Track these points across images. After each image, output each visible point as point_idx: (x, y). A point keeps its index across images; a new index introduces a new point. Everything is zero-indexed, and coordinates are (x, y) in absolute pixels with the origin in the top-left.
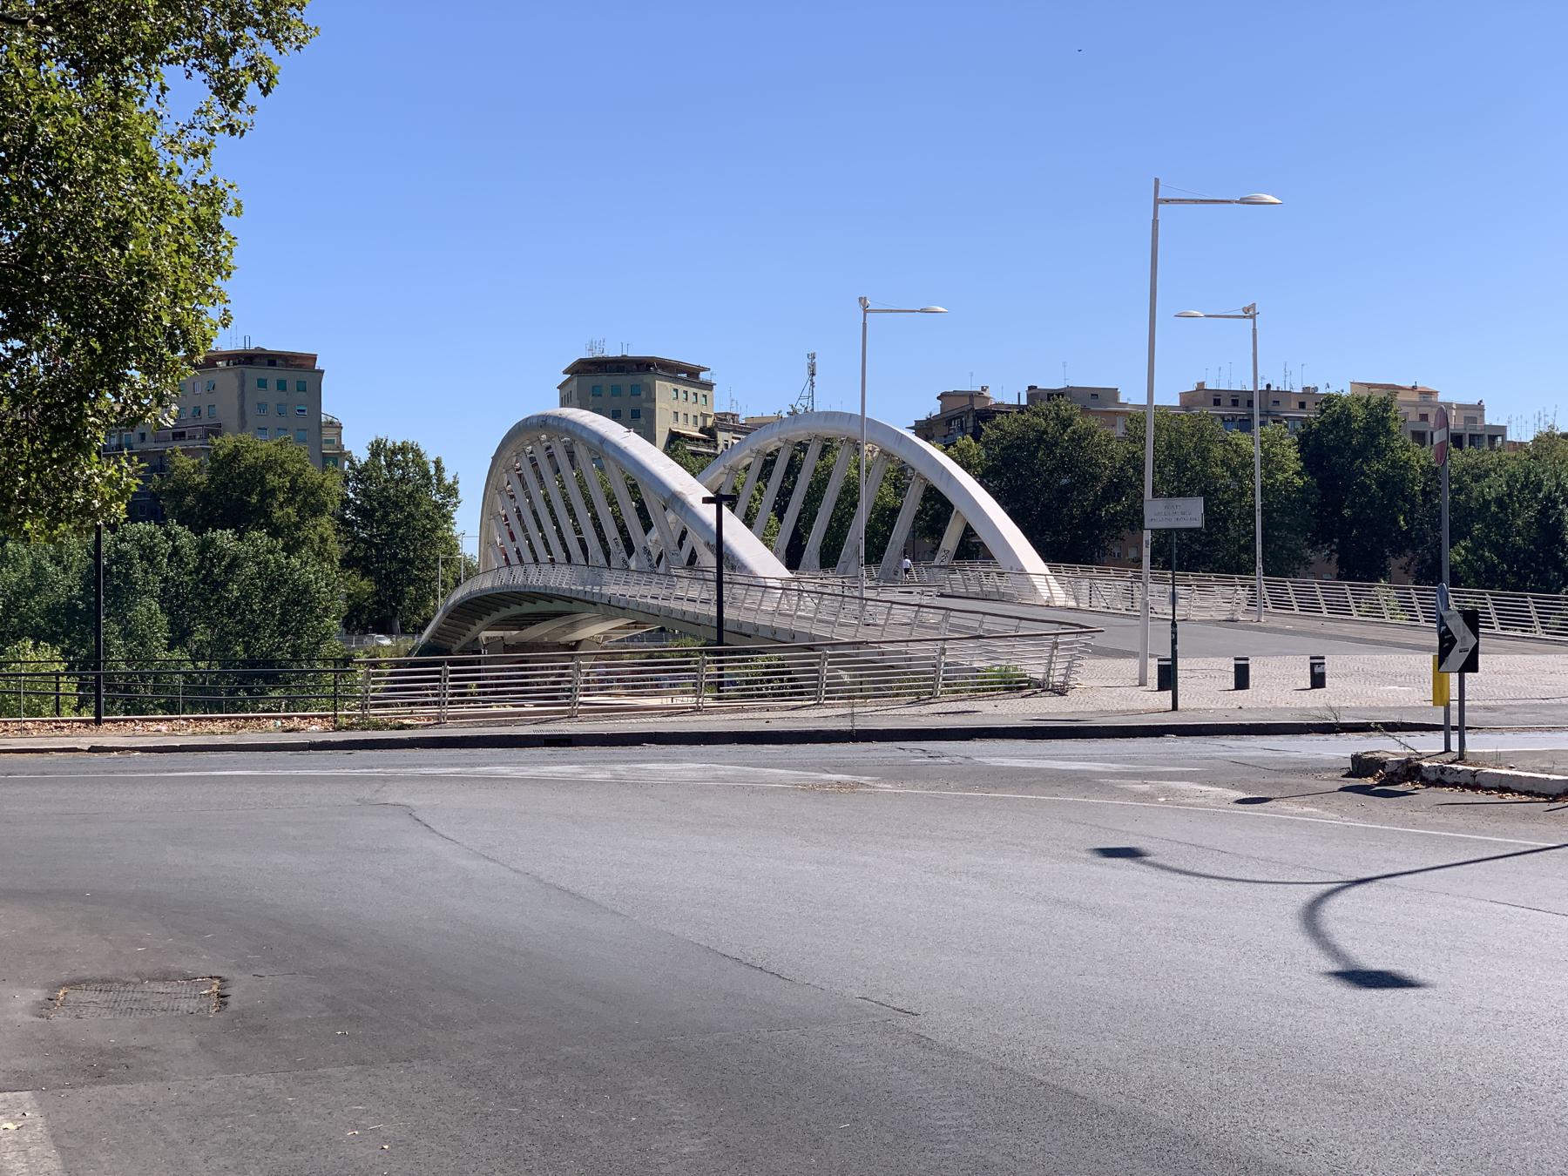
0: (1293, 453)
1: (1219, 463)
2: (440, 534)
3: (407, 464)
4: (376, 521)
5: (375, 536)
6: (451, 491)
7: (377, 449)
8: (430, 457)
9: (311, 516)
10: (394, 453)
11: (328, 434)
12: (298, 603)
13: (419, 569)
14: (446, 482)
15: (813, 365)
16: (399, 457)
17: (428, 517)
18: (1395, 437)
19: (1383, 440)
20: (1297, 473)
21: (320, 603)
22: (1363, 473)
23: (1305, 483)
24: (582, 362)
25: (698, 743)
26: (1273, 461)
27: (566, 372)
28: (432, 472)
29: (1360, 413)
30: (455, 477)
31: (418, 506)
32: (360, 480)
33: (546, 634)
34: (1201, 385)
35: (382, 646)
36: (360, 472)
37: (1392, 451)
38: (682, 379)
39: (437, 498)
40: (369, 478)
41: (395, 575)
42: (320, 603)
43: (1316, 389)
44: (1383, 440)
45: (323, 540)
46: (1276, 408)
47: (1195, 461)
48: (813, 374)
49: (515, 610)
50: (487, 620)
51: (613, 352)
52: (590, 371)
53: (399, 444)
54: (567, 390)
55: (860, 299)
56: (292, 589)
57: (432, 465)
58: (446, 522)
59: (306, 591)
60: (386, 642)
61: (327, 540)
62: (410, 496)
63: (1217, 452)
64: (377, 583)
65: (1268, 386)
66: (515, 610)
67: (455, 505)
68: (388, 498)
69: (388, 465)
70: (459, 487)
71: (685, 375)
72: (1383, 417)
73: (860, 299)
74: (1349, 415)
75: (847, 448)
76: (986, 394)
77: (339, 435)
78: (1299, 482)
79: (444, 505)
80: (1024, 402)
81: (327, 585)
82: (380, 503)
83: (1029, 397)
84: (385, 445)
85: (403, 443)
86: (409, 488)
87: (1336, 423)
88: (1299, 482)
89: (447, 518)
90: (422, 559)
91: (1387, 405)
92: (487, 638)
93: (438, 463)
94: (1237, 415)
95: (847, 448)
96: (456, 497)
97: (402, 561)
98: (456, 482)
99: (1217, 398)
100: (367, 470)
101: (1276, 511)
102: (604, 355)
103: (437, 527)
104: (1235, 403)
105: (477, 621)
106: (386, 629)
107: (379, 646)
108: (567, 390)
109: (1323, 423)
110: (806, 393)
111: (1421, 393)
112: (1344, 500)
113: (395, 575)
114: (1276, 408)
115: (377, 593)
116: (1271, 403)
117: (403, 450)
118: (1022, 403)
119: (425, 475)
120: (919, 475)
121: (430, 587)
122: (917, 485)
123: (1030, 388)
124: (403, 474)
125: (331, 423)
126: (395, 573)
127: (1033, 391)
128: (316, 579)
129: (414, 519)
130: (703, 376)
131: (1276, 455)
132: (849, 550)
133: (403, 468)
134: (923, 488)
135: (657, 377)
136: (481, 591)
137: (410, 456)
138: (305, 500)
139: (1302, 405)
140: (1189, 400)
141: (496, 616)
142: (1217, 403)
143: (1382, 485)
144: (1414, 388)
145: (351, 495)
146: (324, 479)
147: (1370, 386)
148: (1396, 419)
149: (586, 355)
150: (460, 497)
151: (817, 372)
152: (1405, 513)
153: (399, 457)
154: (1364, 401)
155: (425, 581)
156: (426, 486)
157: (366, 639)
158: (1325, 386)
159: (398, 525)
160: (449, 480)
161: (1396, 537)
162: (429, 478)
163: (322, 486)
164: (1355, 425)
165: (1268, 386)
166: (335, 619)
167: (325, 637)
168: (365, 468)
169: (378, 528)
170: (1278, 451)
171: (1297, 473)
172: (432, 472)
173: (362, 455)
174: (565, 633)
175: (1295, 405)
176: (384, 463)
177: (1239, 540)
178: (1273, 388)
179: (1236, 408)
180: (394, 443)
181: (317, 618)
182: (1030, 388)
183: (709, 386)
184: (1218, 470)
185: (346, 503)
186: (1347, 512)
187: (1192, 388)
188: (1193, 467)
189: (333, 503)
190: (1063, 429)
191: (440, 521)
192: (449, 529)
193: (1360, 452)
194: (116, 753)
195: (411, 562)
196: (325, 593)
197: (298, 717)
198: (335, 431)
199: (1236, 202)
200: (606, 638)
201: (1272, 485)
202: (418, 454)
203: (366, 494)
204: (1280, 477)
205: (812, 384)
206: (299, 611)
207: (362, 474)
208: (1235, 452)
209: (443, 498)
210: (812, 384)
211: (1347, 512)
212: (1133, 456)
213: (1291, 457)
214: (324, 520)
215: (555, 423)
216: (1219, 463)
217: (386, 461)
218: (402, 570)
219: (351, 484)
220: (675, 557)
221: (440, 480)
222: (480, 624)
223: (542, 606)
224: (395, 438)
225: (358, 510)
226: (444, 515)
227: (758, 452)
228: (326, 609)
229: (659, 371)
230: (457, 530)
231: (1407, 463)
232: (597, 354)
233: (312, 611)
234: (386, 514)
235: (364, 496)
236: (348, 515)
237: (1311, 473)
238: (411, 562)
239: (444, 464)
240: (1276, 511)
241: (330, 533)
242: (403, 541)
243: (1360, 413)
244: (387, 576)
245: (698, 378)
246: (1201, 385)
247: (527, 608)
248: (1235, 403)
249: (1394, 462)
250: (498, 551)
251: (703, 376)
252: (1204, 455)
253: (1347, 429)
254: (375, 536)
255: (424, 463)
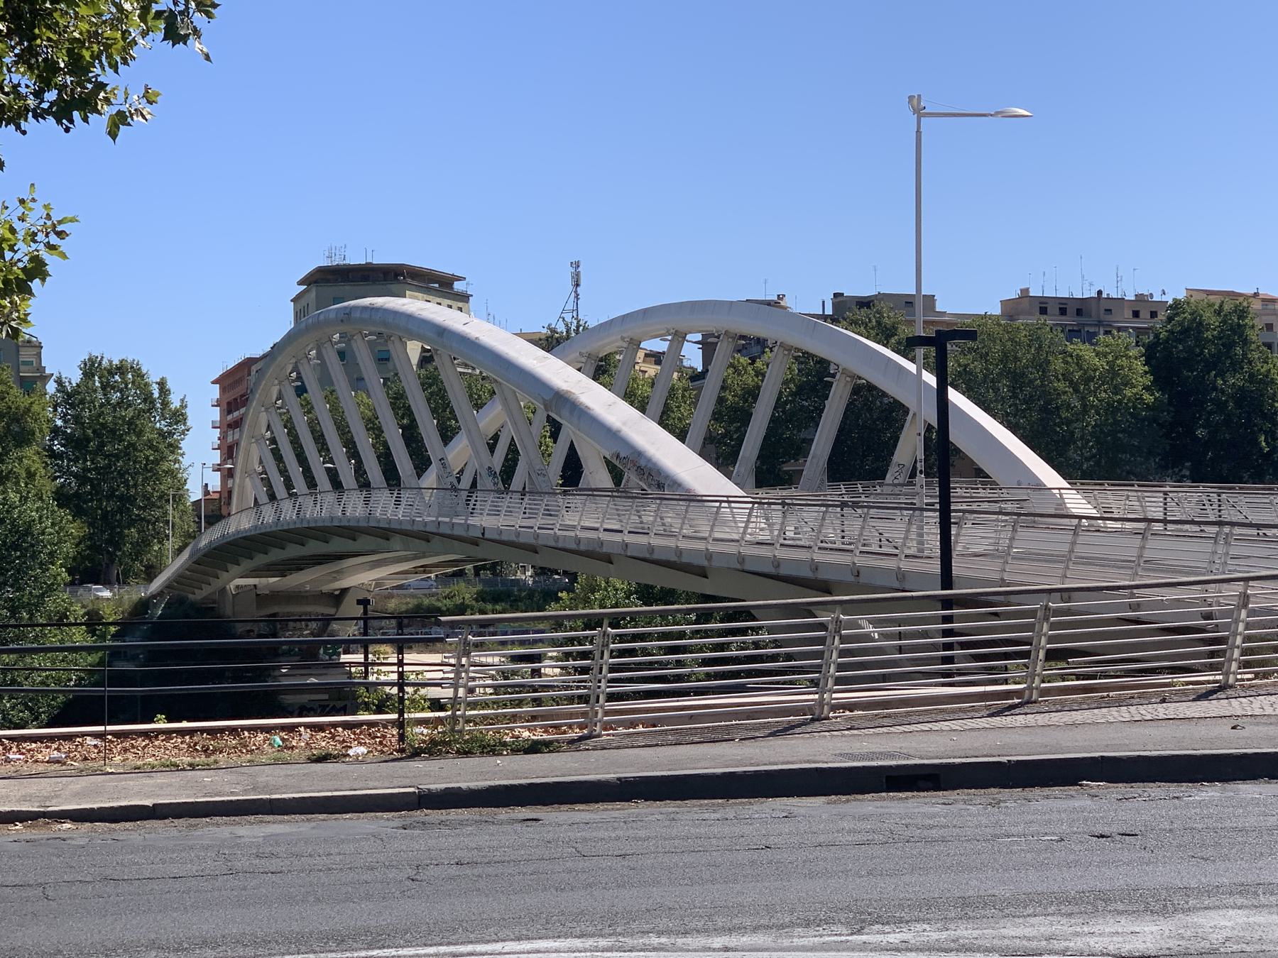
0: (1140, 366)
1: (1060, 377)
2: (165, 466)
3: (126, 387)
4: (90, 453)
5: (89, 470)
6: (179, 417)
7: (90, 368)
8: (153, 378)
9: (16, 447)
10: (111, 372)
11: (26, 354)
12: (16, 547)
13: (140, 508)
14: (173, 407)
15: (578, 274)
16: (117, 377)
17: (151, 447)
18: (1253, 346)
19: (1239, 350)
20: (1146, 388)
21: (45, 546)
22: (1215, 388)
23: (1155, 399)
24: (320, 270)
25: (1193, 779)
26: (1119, 374)
27: (300, 283)
28: (156, 395)
29: (1214, 321)
30: (182, 400)
31: (140, 434)
32: (69, 404)
33: (307, 582)
34: (1025, 292)
35: (102, 599)
36: (69, 395)
37: (1250, 363)
38: (435, 290)
39: (161, 425)
40: (82, 402)
41: (112, 516)
42: (45, 546)
43: (1151, 295)
44: (1239, 350)
45: (31, 475)
46: (1108, 318)
47: (1034, 375)
48: (577, 285)
49: (276, 555)
50: (247, 564)
51: (355, 258)
52: (328, 281)
53: (116, 362)
54: (303, 302)
55: (911, 98)
56: (10, 531)
57: (155, 386)
58: (173, 452)
59: (28, 532)
60: (106, 594)
61: (35, 474)
62: (131, 423)
63: (1058, 365)
64: (91, 525)
65: (1100, 292)
66: (276, 555)
67: (183, 433)
68: (104, 426)
69: (104, 387)
70: (189, 412)
71: (437, 285)
72: (1239, 325)
73: (911, 98)
74: (1200, 323)
75: (725, 344)
76: (782, 303)
77: (39, 355)
78: (1149, 398)
79: (171, 434)
80: (829, 311)
81: (53, 524)
82: (94, 432)
83: (835, 306)
84: (100, 364)
85: (121, 362)
86: (130, 413)
87: (1185, 331)
88: (1149, 398)
89: (174, 447)
90: (144, 496)
91: (1243, 311)
92: (237, 587)
93: (162, 384)
94: (1066, 325)
95: (725, 344)
96: (185, 424)
97: (122, 498)
98: (184, 406)
99: (1043, 306)
100: (79, 393)
101: (1123, 431)
102: (347, 262)
103: (163, 458)
104: (1063, 311)
105: (229, 566)
106: (107, 583)
107: (98, 598)
108: (303, 302)
109: (1171, 332)
110: (570, 306)
111: (1264, 300)
112: (1199, 418)
113: (112, 516)
114: (1108, 318)
115: (91, 537)
116: (1102, 312)
117: (121, 369)
118: (826, 313)
119: (148, 398)
120: (845, 372)
121: (154, 529)
122: (842, 384)
123: (836, 295)
124: (122, 398)
125: (29, 342)
126: (114, 513)
127: (839, 299)
128: (40, 517)
129: (136, 449)
130: (458, 286)
131: (1122, 368)
132: (743, 470)
133: (121, 391)
134: (849, 389)
135: (407, 285)
136: (238, 532)
137: (130, 376)
138: (8, 427)
139: (1136, 314)
140: (1012, 308)
141: (261, 559)
142: (1043, 311)
143: (1239, 404)
144: (1256, 295)
145: (59, 423)
146: (32, 403)
147: (1209, 293)
148: (1253, 327)
149: (325, 263)
150: (189, 423)
151: (582, 282)
152: (1266, 433)
153: (117, 377)
154: (1216, 307)
155: (148, 522)
156: (149, 410)
157: (81, 591)
158: (1160, 293)
159: (118, 457)
160: (175, 403)
161: (1257, 460)
162: (153, 402)
163: (29, 410)
164: (1208, 335)
165: (1100, 292)
166: (61, 565)
167: (51, 589)
168: (76, 391)
169: (92, 462)
170: (1125, 364)
171: (1146, 388)
172: (156, 395)
173: (74, 376)
174: (335, 579)
175: (1128, 314)
176: (97, 384)
177: (1082, 465)
178: (1104, 295)
179: (1064, 318)
180: (111, 362)
181: (41, 564)
182: (836, 295)
183: (464, 297)
184: (1061, 386)
185: (56, 431)
186: (1200, 433)
187: (1014, 294)
188: (1031, 381)
189: (41, 430)
190: (886, 339)
191: (167, 452)
192: (176, 461)
193: (1213, 364)
194: (19, 826)
195: (131, 500)
196: (50, 534)
197: (307, 726)
198: (34, 351)
199: (991, 115)
200: (377, 585)
201: (1120, 402)
202: (138, 374)
203: (77, 419)
204: (1128, 392)
205: (577, 297)
206: (18, 558)
207: (71, 398)
208: (1077, 364)
209: (170, 425)
210: (577, 297)
211: (1200, 433)
212: (965, 370)
213: (1138, 372)
214: (29, 451)
215: (366, 316)
216: (1060, 377)
217: (101, 382)
218: (120, 511)
219: (60, 410)
220: (540, 478)
221: (165, 404)
222: (234, 569)
223: (314, 547)
224: (112, 355)
225: (69, 441)
226: (170, 445)
227: (589, 356)
228: (51, 554)
229: (409, 281)
230: (185, 461)
231: (1267, 376)
232: (337, 261)
233: (34, 557)
234: (102, 445)
235: (76, 423)
236: (57, 447)
237: (1161, 389)
238: (131, 500)
239: (169, 385)
240: (1123, 431)
241: (37, 466)
242: (121, 475)
243: (1214, 321)
244: (105, 514)
245: (453, 288)
246: (1025, 292)
247: (293, 551)
248: (1063, 311)
249: (1252, 375)
250: (258, 482)
251: (458, 286)
252: (1043, 366)
253: (1199, 340)
254: (89, 470)
255: (147, 385)
